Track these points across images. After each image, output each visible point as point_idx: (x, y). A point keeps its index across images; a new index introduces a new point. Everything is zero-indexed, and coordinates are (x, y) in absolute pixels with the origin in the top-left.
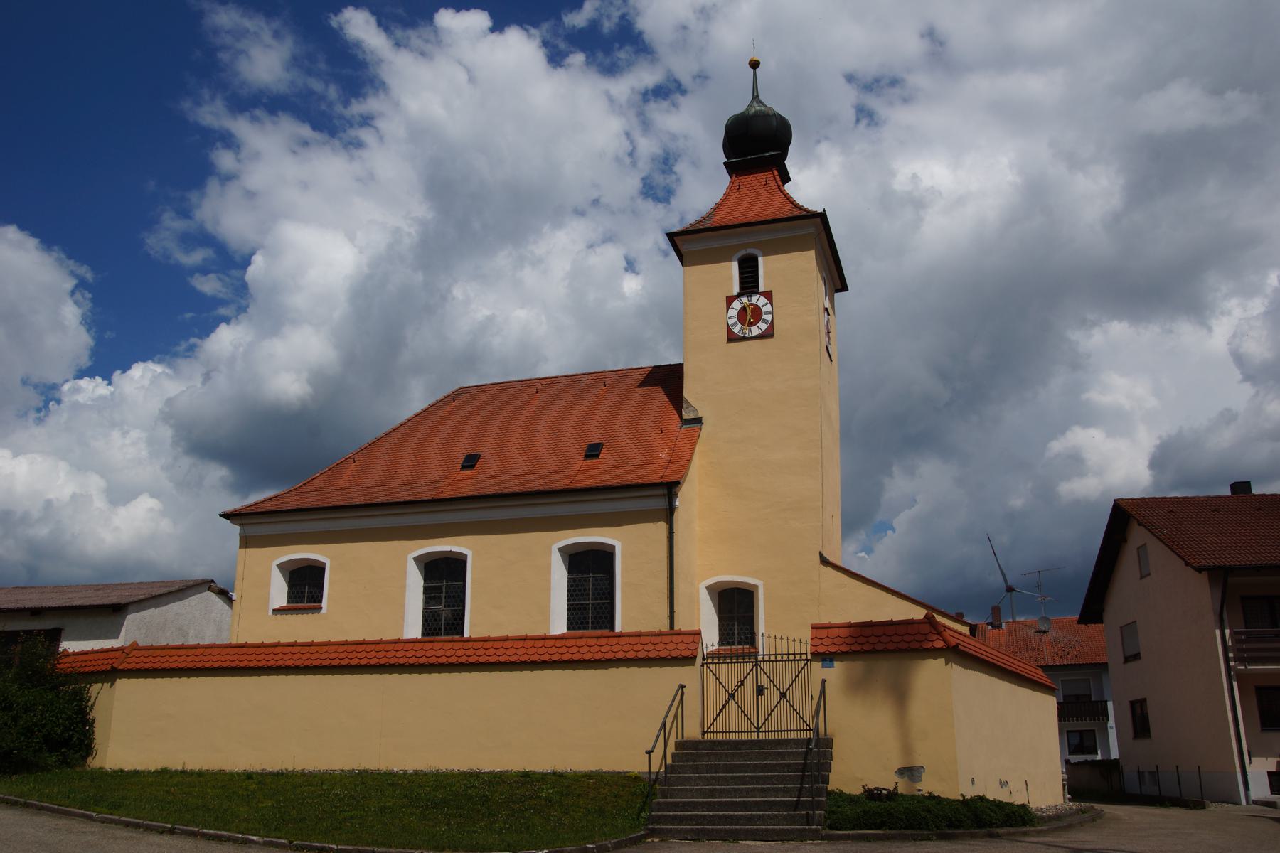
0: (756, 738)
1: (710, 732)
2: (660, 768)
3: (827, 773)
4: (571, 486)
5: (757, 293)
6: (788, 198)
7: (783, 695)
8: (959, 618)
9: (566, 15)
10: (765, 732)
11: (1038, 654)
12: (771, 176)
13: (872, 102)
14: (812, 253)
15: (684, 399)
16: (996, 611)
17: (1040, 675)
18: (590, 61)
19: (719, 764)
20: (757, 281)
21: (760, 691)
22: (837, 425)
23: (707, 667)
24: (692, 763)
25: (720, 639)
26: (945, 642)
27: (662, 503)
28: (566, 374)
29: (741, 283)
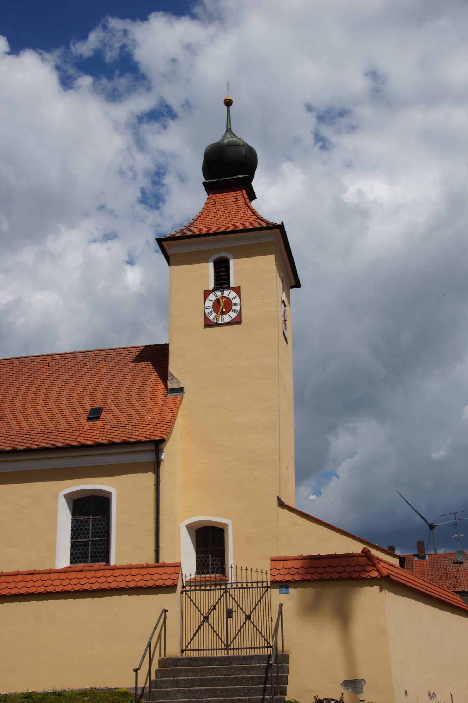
0: (226, 655)
2: (146, 684)
3: (285, 685)
4: (76, 443)
5: (228, 288)
6: (254, 213)
7: (248, 617)
8: (390, 551)
9: (74, 44)
10: (234, 649)
11: (456, 582)
12: (240, 195)
13: (326, 131)
14: (272, 257)
15: (169, 373)
16: (420, 545)
17: (457, 600)
18: (95, 89)
19: (195, 679)
20: (228, 279)
21: (229, 614)
22: (291, 394)
23: (186, 593)
24: (172, 678)
25: (197, 569)
26: (379, 573)
27: (150, 457)
28: (73, 351)
29: (216, 280)
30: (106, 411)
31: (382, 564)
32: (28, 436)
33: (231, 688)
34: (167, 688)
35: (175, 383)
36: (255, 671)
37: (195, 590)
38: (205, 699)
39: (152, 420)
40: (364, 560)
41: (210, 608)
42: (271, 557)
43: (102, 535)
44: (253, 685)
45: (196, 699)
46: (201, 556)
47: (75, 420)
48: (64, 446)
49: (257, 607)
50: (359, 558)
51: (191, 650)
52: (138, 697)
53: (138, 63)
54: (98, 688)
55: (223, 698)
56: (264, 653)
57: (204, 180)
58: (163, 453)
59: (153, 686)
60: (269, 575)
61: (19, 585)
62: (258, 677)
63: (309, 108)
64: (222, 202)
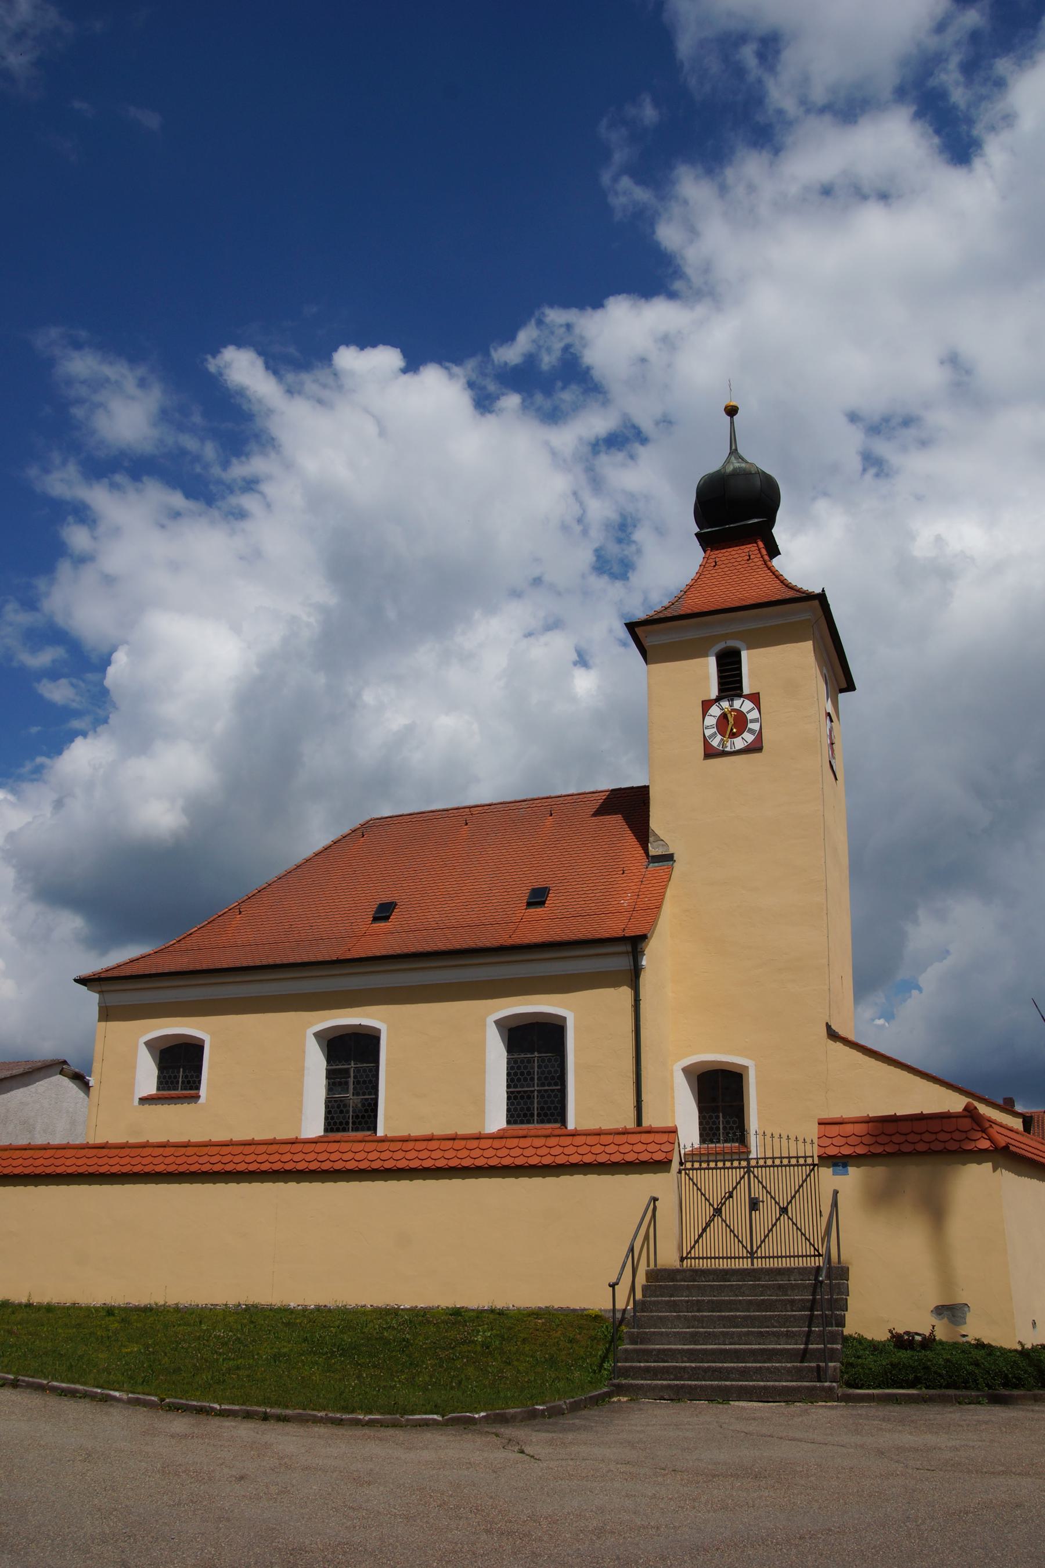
1: (691, 1258)
2: (627, 1304)
3: (843, 1313)
4: (510, 942)
5: (740, 696)
6: (778, 576)
7: (784, 1210)
8: (1007, 1107)
9: (496, 350)
10: (761, 1258)
12: (755, 550)
13: (882, 448)
14: (809, 644)
15: (650, 831)
20: (740, 681)
21: (754, 1205)
22: (845, 860)
23: (686, 1173)
24: (667, 1299)
26: (992, 1142)
27: (624, 963)
30: (555, 892)
31: (996, 1128)
32: (438, 932)
33: (758, 1315)
34: (660, 1312)
35: (661, 847)
36: (796, 1291)
37: (700, 1169)
38: (719, 1330)
39: (625, 905)
40: (967, 1123)
41: (725, 1196)
42: (819, 1119)
43: (552, 1082)
44: (793, 1311)
45: (705, 1330)
46: (707, 1115)
47: (508, 906)
48: (493, 946)
49: (797, 1195)
50: (959, 1119)
51: (695, 1258)
52: (617, 1323)
53: (588, 369)
54: (556, 1307)
55: (746, 1330)
56: (809, 1265)
57: (697, 530)
58: (645, 957)
59: (638, 1308)
60: (815, 1146)
61: (434, 1155)
62: (800, 1300)
63: (853, 417)
64: (727, 562)
